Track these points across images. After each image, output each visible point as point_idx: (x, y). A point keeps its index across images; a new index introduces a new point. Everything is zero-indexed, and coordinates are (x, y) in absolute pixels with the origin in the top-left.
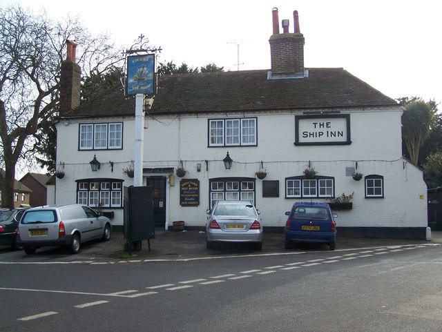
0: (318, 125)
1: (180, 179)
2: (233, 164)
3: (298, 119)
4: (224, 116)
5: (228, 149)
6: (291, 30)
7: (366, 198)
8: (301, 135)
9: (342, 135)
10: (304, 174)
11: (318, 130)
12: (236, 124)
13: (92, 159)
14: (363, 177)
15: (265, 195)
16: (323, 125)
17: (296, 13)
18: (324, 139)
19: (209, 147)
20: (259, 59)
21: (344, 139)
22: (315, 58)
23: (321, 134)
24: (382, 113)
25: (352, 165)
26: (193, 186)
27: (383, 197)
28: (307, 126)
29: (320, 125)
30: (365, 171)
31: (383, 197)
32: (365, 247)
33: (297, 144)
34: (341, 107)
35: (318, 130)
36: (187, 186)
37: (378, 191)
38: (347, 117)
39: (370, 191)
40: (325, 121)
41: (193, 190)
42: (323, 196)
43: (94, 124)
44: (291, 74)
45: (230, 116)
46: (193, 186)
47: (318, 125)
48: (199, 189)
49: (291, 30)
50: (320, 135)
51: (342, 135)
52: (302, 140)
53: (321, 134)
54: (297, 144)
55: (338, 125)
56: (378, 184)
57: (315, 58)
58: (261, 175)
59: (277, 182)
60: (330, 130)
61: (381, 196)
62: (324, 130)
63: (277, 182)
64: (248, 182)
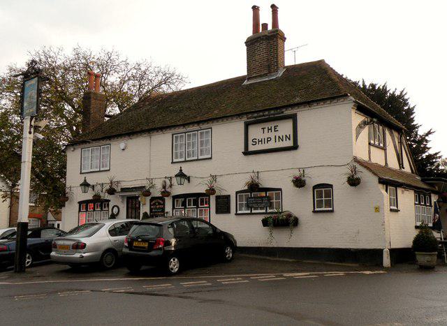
0: (266, 130)
1: (148, 199)
2: (191, 179)
3: (247, 125)
4: (184, 130)
5: (85, 175)
6: (270, 28)
7: (314, 212)
8: (250, 142)
9: (289, 139)
10: (246, 188)
11: (267, 135)
12: (192, 139)
13: (82, 181)
14: (151, 196)
15: (218, 212)
16: (271, 129)
17: (274, 8)
18: (272, 145)
19: (172, 163)
20: (235, 65)
21: (290, 143)
22: (295, 54)
23: (269, 140)
24: (330, 108)
25: (297, 174)
26: (160, 204)
27: (332, 211)
28: (256, 132)
29: (269, 129)
30: (314, 178)
31: (332, 211)
32: (259, 273)
33: (247, 153)
34: (286, 107)
35: (267, 135)
36: (154, 204)
37: (329, 203)
38: (294, 118)
39: (320, 204)
40: (271, 125)
41: (159, 208)
42: (320, 209)
43: (185, 133)
44: (266, 75)
45: (189, 129)
46: (160, 204)
47: (266, 130)
48: (164, 206)
49: (270, 28)
50: (268, 141)
51: (289, 139)
52: (251, 148)
53: (269, 140)
54: (247, 153)
55: (285, 128)
56: (329, 194)
57: (295, 54)
58: (211, 191)
59: (228, 197)
60: (278, 134)
61: (331, 209)
62: (272, 135)
63: (228, 197)
64: (323, 190)
